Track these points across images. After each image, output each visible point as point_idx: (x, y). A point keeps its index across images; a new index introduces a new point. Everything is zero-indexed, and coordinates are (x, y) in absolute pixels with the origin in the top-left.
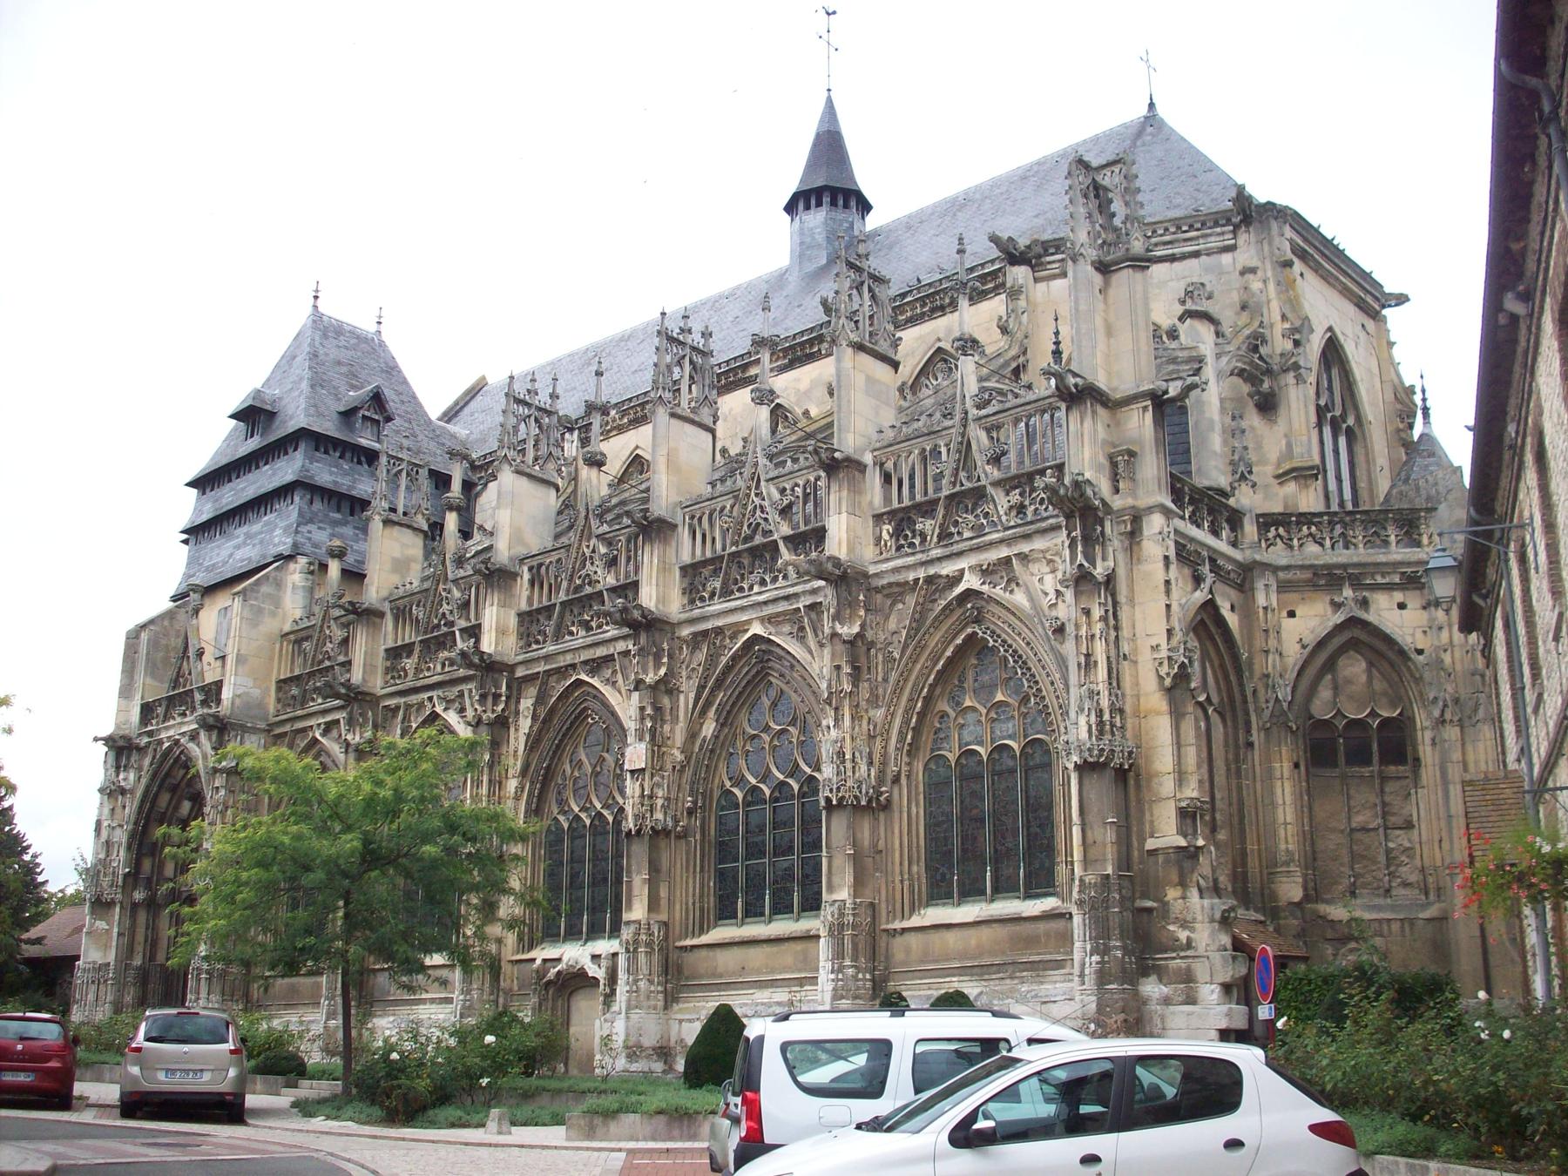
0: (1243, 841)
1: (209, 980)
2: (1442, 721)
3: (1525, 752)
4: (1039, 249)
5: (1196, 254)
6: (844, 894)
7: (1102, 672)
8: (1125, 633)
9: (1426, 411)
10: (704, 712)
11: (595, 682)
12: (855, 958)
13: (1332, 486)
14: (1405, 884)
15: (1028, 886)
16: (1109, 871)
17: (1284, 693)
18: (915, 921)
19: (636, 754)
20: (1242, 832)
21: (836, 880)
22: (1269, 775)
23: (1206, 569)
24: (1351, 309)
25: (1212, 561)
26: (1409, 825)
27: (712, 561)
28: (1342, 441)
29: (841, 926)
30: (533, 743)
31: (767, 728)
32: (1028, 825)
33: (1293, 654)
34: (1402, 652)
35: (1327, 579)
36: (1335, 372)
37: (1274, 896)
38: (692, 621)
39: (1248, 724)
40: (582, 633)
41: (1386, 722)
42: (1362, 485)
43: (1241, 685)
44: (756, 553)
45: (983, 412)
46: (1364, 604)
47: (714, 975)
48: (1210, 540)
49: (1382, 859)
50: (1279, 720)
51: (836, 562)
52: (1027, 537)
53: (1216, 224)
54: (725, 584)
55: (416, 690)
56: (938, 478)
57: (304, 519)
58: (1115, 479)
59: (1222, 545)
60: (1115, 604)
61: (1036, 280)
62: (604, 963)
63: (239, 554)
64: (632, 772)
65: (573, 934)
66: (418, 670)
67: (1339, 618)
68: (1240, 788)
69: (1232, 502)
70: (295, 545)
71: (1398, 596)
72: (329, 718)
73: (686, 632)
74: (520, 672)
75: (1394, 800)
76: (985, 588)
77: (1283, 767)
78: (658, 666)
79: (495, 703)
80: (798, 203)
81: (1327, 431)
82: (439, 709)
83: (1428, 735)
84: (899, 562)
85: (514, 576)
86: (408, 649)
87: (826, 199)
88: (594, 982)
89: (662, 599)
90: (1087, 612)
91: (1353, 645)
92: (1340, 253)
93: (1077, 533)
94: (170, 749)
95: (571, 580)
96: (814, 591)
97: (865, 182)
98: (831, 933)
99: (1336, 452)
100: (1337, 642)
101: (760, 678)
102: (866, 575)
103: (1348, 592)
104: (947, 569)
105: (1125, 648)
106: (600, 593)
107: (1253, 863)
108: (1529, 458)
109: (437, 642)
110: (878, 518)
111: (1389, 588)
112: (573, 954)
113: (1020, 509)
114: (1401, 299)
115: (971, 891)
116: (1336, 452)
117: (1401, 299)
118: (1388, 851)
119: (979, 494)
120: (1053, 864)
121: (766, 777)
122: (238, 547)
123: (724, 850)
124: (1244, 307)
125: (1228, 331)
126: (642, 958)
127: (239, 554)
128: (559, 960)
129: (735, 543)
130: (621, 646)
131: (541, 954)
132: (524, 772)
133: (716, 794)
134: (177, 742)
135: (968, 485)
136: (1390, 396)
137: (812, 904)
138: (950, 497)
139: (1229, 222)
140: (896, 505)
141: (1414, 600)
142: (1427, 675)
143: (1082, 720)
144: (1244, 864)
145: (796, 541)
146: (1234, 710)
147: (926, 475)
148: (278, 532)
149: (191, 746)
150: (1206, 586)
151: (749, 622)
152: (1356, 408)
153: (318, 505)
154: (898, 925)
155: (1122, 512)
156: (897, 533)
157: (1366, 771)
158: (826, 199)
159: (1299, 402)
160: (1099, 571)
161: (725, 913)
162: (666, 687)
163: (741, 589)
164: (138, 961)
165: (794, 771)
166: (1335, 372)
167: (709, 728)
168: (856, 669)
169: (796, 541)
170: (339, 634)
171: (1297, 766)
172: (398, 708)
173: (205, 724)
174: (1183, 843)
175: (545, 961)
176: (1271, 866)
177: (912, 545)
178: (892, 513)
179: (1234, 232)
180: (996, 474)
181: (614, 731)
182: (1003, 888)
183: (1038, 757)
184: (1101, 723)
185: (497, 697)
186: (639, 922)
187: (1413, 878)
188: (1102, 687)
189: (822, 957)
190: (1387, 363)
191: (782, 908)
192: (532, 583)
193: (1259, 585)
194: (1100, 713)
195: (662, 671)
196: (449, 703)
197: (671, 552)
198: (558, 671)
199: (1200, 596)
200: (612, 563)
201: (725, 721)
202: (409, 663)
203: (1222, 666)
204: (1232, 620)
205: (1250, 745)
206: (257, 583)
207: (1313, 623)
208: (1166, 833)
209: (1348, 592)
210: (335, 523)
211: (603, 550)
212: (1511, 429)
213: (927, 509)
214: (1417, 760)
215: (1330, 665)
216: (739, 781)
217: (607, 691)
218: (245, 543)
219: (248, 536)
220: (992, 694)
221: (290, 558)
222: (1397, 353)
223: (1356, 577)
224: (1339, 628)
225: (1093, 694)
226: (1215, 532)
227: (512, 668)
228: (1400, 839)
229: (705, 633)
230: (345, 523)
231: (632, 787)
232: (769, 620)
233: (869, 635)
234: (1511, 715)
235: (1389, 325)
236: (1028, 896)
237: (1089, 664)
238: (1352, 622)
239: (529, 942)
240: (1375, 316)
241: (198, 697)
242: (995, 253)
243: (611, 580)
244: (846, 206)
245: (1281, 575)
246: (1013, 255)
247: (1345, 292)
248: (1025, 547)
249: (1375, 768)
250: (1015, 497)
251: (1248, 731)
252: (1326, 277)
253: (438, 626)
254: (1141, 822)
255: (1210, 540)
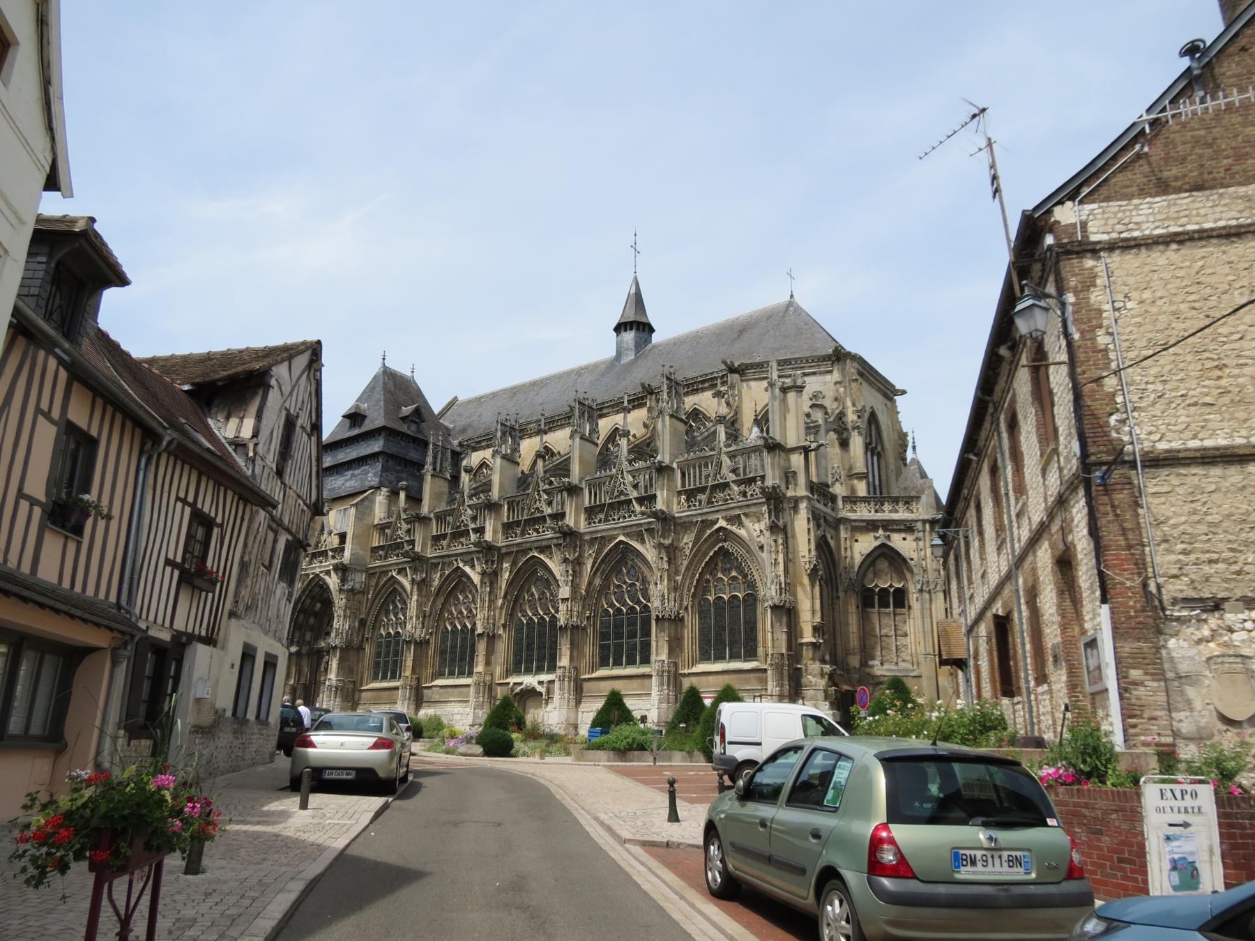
0: (835, 639)
1: (336, 692)
2: (921, 591)
3: (963, 613)
4: (743, 367)
5: (814, 373)
6: (664, 657)
7: (781, 567)
8: (790, 550)
9: (914, 448)
10: (595, 573)
11: (542, 557)
12: (668, 686)
13: (871, 480)
14: (904, 661)
15: (745, 657)
16: (784, 651)
17: (853, 576)
18: (694, 670)
19: (565, 592)
20: (835, 634)
21: (660, 651)
22: (846, 612)
23: (822, 521)
24: (880, 397)
25: (825, 517)
26: (905, 635)
27: (600, 506)
28: (875, 458)
29: (663, 672)
30: (511, 584)
31: (625, 582)
32: (745, 628)
33: (858, 560)
34: (904, 560)
35: (871, 526)
36: (873, 427)
37: (848, 665)
38: (590, 533)
39: (837, 588)
40: (535, 534)
41: (897, 590)
42: (883, 478)
43: (835, 571)
44: (621, 503)
45: (729, 449)
46: (888, 538)
47: (598, 691)
48: (823, 508)
49: (894, 649)
50: (851, 587)
51: (662, 512)
52: (748, 506)
53: (824, 360)
54: (606, 516)
55: (448, 556)
56: (707, 476)
57: (384, 469)
58: (787, 483)
59: (828, 511)
60: (786, 537)
61: (742, 381)
62: (545, 685)
63: (348, 484)
64: (562, 600)
65: (528, 671)
66: (449, 546)
67: (877, 543)
68: (834, 617)
69: (831, 490)
70: (380, 482)
71: (903, 535)
72: (400, 567)
73: (587, 538)
74: (504, 551)
75: (900, 625)
76: (729, 527)
77: (852, 608)
78: (575, 552)
79: (492, 564)
80: (620, 328)
81: (869, 454)
82: (461, 565)
83: (915, 596)
84: (689, 513)
85: (501, 506)
86: (444, 536)
87: (635, 327)
88: (541, 694)
89: (576, 522)
90: (775, 541)
91: (883, 555)
92: (876, 372)
93: (772, 507)
94: (313, 578)
95: (529, 509)
96: (650, 523)
97: (653, 318)
98: (658, 675)
99: (873, 464)
100: (876, 553)
101: (623, 560)
102: (674, 517)
103: (881, 532)
104: (711, 517)
105: (790, 556)
106: (544, 517)
107: (839, 649)
108: (972, 504)
109: (460, 534)
110: (680, 493)
111: (899, 531)
112: (529, 680)
113: (744, 494)
114: (903, 392)
115: (720, 657)
116: (873, 464)
117: (903, 392)
118: (897, 646)
119: (725, 486)
120: (756, 646)
121: (625, 604)
122: (347, 481)
123: (604, 636)
124: (836, 399)
125: (829, 411)
126: (566, 683)
127: (348, 484)
128: (521, 684)
129: (611, 499)
130: (555, 541)
131: (513, 680)
132: (505, 597)
133: (600, 611)
134: (317, 575)
135: (721, 481)
136: (896, 437)
137: (646, 661)
138: (713, 486)
139: (830, 359)
140: (687, 488)
141: (910, 538)
142: (915, 570)
143: (773, 587)
144: (835, 649)
145: (640, 500)
146: (831, 582)
147: (700, 475)
148: (370, 475)
149: (326, 578)
150: (822, 529)
151: (618, 535)
152: (882, 442)
153: (390, 463)
154: (686, 671)
155: (790, 498)
156: (688, 500)
157: (887, 610)
158: (635, 327)
159: (857, 443)
160: (781, 524)
161: (604, 663)
162: (578, 562)
163: (614, 520)
164: (292, 682)
165: (638, 603)
166: (873, 427)
167: (597, 581)
168: (669, 559)
169: (640, 500)
170: (405, 526)
171: (858, 607)
172: (438, 563)
173: (337, 568)
174: (814, 641)
175: (515, 684)
176: (847, 652)
177: (695, 505)
178: (686, 491)
179: (832, 364)
180: (733, 477)
181: (549, 582)
182: (734, 656)
183: (752, 600)
184: (781, 589)
185: (493, 562)
186: (565, 667)
187: (908, 658)
188: (782, 574)
189: (653, 684)
190: (896, 423)
191: (631, 662)
192: (509, 509)
193: (842, 527)
194: (780, 584)
195: (577, 554)
196: (466, 563)
197: (580, 500)
198: (523, 551)
199: (820, 533)
200: (550, 503)
201: (607, 579)
202: (444, 543)
203: (827, 563)
204: (832, 543)
205: (838, 598)
206: (363, 500)
207: (867, 544)
208: (808, 637)
209: (881, 532)
210: (398, 472)
211: (546, 497)
212: (965, 491)
213: (702, 490)
214: (910, 607)
215: (873, 563)
216: (612, 605)
217: (547, 561)
218: (351, 479)
219: (353, 475)
220: (730, 573)
221: (378, 488)
222: (900, 417)
223: (889, 526)
224: (877, 548)
225: (778, 576)
226: (825, 505)
227: (499, 549)
228: (901, 641)
229: (596, 538)
230: (402, 471)
231: (562, 607)
232: (626, 535)
233: (675, 544)
234: (956, 595)
235: (897, 404)
236: (745, 661)
237: (776, 563)
238: (883, 545)
239: (508, 673)
240: (891, 400)
241: (330, 553)
242: (723, 367)
243: (550, 511)
244: (644, 330)
245: (853, 524)
246: (732, 370)
247: (879, 390)
248: (747, 510)
249: (891, 609)
250: (742, 488)
251: (837, 591)
252: (871, 384)
253: (460, 526)
254: (796, 632)
255: (823, 508)
